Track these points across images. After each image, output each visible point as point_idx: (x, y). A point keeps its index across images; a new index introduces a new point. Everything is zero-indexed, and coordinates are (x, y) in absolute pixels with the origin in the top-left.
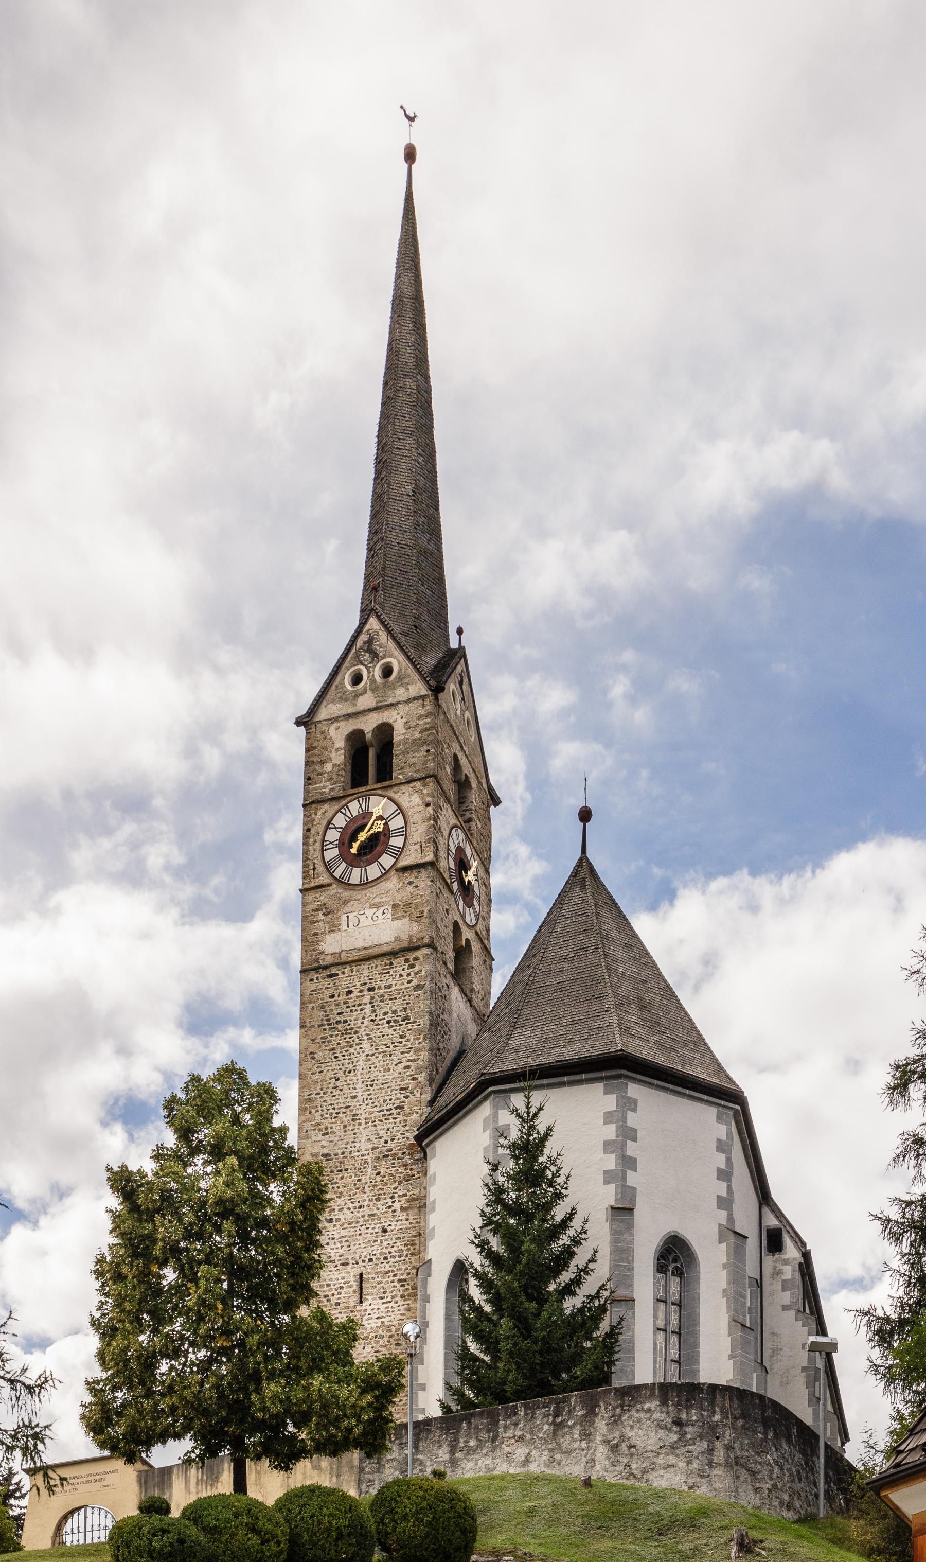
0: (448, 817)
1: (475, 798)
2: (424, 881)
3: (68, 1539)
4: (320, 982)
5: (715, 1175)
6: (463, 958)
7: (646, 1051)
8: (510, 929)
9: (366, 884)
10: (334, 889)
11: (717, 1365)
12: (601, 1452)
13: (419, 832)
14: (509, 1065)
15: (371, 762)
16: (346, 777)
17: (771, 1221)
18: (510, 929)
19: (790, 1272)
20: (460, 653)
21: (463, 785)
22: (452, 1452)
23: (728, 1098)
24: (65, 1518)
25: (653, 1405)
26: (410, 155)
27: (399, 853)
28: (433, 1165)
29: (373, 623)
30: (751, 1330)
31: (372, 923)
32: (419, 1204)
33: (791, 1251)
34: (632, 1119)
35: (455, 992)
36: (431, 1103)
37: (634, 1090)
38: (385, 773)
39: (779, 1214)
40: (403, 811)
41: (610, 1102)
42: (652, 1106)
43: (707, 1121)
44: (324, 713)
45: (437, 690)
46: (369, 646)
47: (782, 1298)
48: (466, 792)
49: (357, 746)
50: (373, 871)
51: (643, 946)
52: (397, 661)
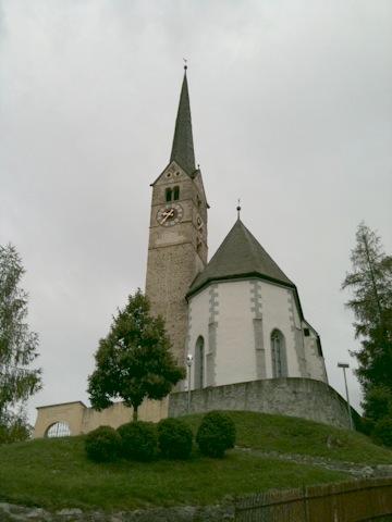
0: (195, 210)
1: (202, 206)
2: (188, 226)
3: (50, 435)
4: (154, 252)
5: (343, 307)
6: (201, 246)
7: (262, 272)
8: (215, 240)
9: (170, 226)
10: (161, 228)
11: (293, 370)
12: (265, 403)
13: (187, 213)
14: (218, 275)
15: (172, 195)
16: (165, 199)
17: (305, 326)
18: (215, 240)
19: (313, 343)
20: (199, 171)
21: (199, 203)
22: (206, 402)
23: (292, 287)
24: (50, 427)
25: (284, 385)
26: (186, 68)
27: (180, 218)
28: (191, 305)
29: (174, 162)
30: (302, 360)
31: (172, 237)
32: (186, 318)
33: (313, 336)
34: (259, 292)
35: (197, 256)
36: (191, 287)
37: (260, 283)
38: (176, 198)
39: (307, 324)
40: (183, 207)
41: (252, 287)
42: (266, 289)
43: (283, 295)
44: (158, 184)
45: (193, 178)
46: (173, 168)
47: (311, 351)
48: (201, 205)
49: (168, 193)
50: (172, 223)
51: (149, 273)
52: (181, 172)
